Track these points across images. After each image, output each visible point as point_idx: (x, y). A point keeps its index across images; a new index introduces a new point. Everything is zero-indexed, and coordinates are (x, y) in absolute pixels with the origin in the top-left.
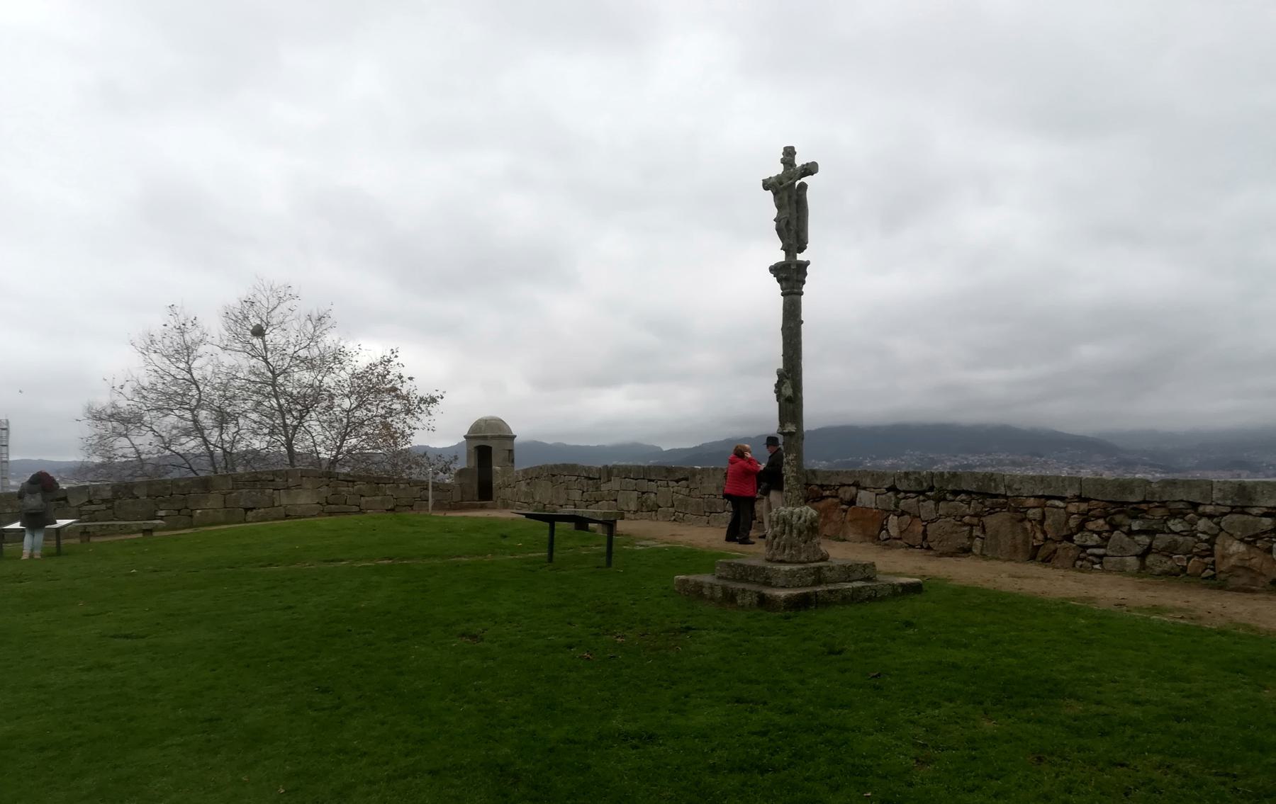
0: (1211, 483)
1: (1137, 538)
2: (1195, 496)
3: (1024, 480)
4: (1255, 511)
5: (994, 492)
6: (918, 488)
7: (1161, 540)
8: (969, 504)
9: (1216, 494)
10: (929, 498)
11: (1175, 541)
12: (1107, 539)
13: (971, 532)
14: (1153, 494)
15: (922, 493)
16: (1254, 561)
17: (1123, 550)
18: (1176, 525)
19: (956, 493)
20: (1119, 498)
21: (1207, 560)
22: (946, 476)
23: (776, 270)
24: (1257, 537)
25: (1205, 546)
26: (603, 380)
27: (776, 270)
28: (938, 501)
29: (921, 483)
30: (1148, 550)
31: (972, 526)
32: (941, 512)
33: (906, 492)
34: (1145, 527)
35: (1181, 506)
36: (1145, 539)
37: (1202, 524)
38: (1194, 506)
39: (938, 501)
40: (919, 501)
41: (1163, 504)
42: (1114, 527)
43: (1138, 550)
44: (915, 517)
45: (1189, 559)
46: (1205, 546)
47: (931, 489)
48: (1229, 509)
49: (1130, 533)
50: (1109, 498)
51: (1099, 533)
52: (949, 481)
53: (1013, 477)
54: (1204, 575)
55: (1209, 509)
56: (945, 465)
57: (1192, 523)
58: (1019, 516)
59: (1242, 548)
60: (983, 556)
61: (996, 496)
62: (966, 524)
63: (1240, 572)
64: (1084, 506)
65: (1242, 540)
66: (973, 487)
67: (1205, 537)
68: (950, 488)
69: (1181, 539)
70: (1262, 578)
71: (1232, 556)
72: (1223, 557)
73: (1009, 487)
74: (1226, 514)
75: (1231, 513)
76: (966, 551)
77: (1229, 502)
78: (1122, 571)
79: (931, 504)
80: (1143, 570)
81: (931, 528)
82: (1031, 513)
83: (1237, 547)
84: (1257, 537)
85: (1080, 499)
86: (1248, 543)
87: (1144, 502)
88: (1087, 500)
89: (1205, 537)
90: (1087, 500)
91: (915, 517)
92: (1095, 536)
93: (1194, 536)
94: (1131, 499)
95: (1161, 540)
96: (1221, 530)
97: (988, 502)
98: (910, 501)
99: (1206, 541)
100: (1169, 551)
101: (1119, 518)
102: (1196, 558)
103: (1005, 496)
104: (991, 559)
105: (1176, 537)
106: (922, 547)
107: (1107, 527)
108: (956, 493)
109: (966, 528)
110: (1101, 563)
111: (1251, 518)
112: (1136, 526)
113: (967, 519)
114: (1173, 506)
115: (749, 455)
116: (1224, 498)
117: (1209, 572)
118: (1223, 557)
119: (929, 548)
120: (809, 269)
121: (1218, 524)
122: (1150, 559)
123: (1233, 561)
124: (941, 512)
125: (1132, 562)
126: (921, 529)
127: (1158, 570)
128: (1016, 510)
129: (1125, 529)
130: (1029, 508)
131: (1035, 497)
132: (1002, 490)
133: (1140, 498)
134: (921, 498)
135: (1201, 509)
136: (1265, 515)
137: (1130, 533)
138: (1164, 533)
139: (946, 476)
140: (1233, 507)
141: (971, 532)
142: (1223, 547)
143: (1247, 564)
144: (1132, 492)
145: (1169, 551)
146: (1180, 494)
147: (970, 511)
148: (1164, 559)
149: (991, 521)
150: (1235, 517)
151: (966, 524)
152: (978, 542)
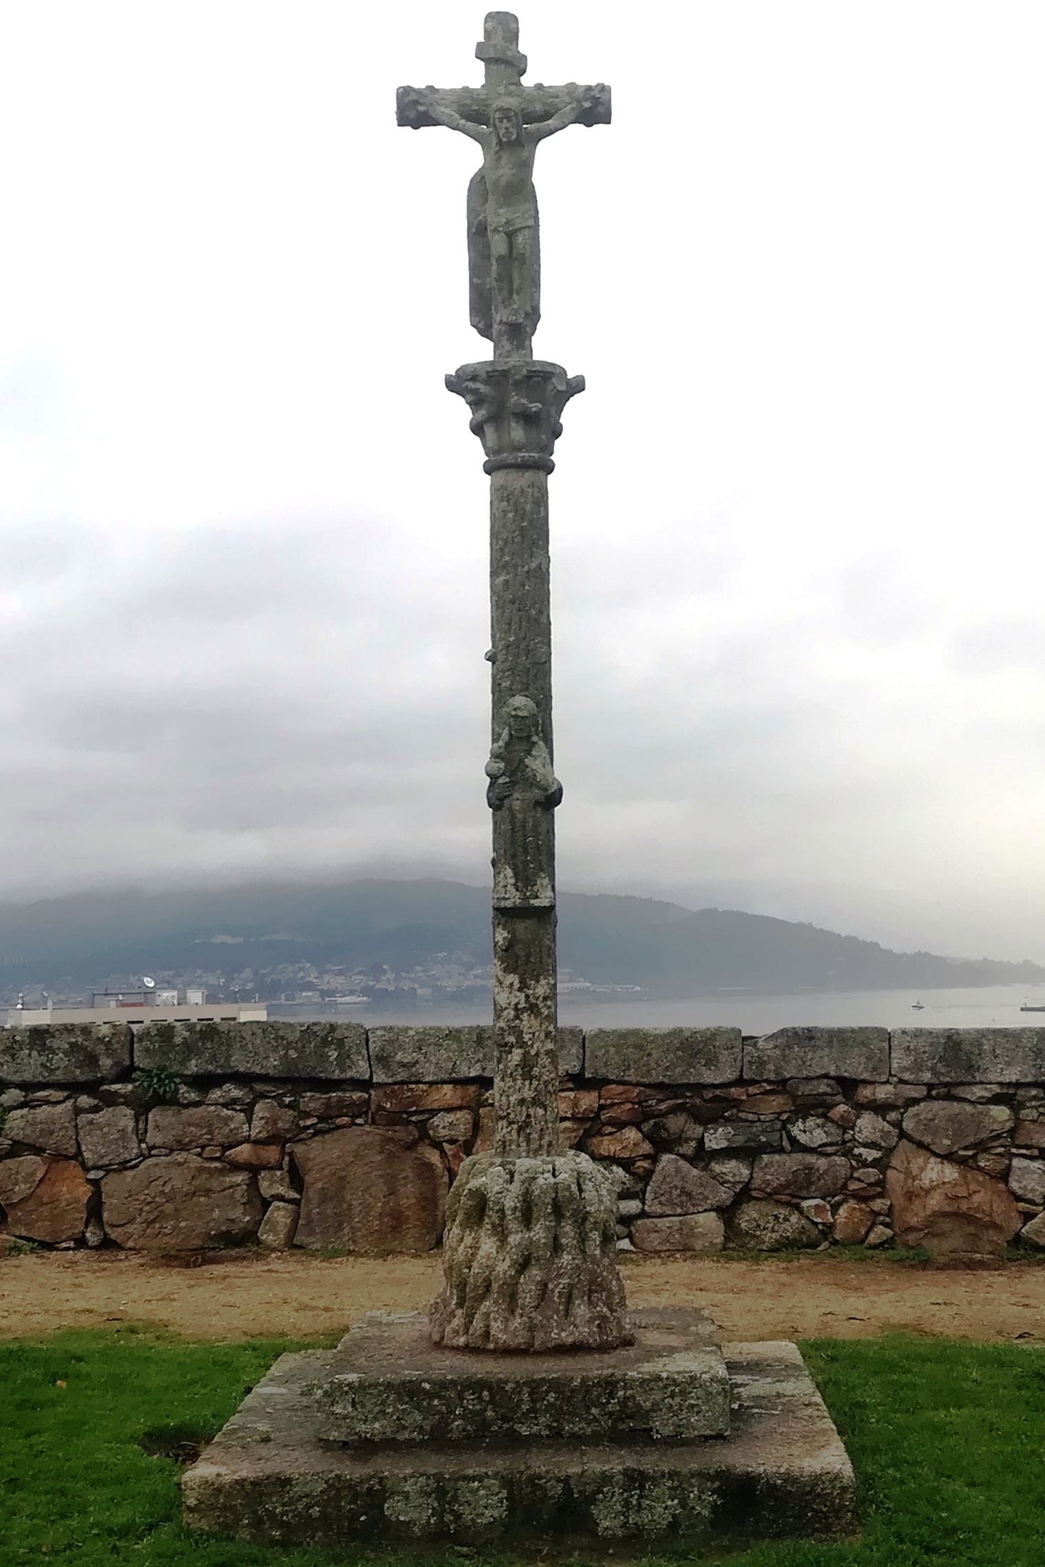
0: (889, 1037)
1: (717, 1167)
2: (854, 1067)
3: (423, 1041)
4: (979, 1092)
5: (337, 1075)
6: (80, 1075)
7: (776, 1168)
8: (249, 1111)
9: (899, 1060)
10: (111, 1100)
11: (809, 1168)
12: (649, 1173)
13: (253, 1184)
14: (762, 1063)
15: (90, 1087)
16: (977, 1198)
17: (687, 1199)
18: (811, 1132)
19: (204, 1082)
20: (678, 1075)
21: (878, 1204)
22: (181, 1034)
23: (462, 383)
24: (981, 1147)
25: (873, 1174)
26: (773, 1336)
27: (462, 383)
28: (141, 1108)
29: (91, 1060)
30: (744, 1194)
31: (254, 1169)
32: (153, 1137)
33: (25, 1086)
34: (740, 1140)
35: (823, 1088)
36: (734, 1169)
37: (868, 1126)
38: (848, 1086)
39: (141, 1108)
40: (77, 1111)
41: (781, 1085)
42: (662, 1143)
43: (724, 1195)
44: (59, 1157)
45: (835, 1208)
46: (873, 1174)
47: (125, 1074)
48: (923, 1091)
49: (702, 1156)
50: (657, 1077)
51: (626, 1164)
52: (189, 1049)
53: (394, 1036)
54: (872, 1238)
55: (883, 1093)
56: (181, 1003)
57: (846, 1125)
58: (400, 1133)
59: (950, 1173)
60: (292, 1245)
61: (337, 1084)
62: (236, 1167)
63: (946, 1225)
64: (588, 1100)
65: (948, 1157)
66: (272, 1064)
67: (871, 1155)
68: (193, 1067)
69: (821, 1163)
70: (992, 1235)
71: (928, 1192)
72: (910, 1196)
73: (383, 1060)
74: (915, 1101)
75: (929, 1097)
76: (239, 1243)
77: (927, 1076)
78: (686, 1249)
79: (124, 1117)
80: (736, 1243)
81: (111, 1185)
82: (442, 1124)
83: (936, 1173)
84: (981, 1147)
85: (578, 1081)
86: (961, 1162)
87: (740, 1082)
88: (597, 1084)
89: (871, 1155)
90: (597, 1084)
91: (59, 1157)
92: (619, 1171)
93: (848, 1153)
94: (709, 1077)
95: (776, 1168)
96: (903, 1135)
97: (312, 1101)
98: (44, 1112)
99: (875, 1163)
100: (789, 1194)
101: (676, 1123)
102: (852, 1203)
103: (366, 1085)
104: (313, 1255)
105: (811, 1159)
106: (81, 1243)
107: (647, 1148)
108: (204, 1082)
109: (240, 1178)
110: (630, 1236)
111: (968, 1108)
112: (716, 1139)
113: (243, 1152)
114: (805, 1089)
115: (664, 1375)
116: (918, 1067)
117: (880, 1233)
118: (910, 1196)
119: (107, 1245)
120: (572, 414)
121: (898, 1124)
122: (749, 1215)
123: (935, 1202)
124: (153, 1137)
125: (709, 1223)
126: (84, 1192)
127: (769, 1238)
128: (394, 1119)
129: (689, 1148)
130: (434, 1112)
131: (455, 1082)
132: (360, 1069)
133: (730, 1075)
134: (85, 1100)
135: (865, 1093)
136: (996, 1100)
137: (702, 1156)
138: (781, 1150)
139: (181, 1034)
140: (930, 1086)
141: (253, 1184)
142: (908, 1173)
143: (964, 1206)
144: (711, 1062)
145: (789, 1194)
146: (825, 1062)
147: (257, 1129)
148: (783, 1212)
149: (320, 1154)
150: (936, 1106)
151: (236, 1167)
152: (279, 1215)
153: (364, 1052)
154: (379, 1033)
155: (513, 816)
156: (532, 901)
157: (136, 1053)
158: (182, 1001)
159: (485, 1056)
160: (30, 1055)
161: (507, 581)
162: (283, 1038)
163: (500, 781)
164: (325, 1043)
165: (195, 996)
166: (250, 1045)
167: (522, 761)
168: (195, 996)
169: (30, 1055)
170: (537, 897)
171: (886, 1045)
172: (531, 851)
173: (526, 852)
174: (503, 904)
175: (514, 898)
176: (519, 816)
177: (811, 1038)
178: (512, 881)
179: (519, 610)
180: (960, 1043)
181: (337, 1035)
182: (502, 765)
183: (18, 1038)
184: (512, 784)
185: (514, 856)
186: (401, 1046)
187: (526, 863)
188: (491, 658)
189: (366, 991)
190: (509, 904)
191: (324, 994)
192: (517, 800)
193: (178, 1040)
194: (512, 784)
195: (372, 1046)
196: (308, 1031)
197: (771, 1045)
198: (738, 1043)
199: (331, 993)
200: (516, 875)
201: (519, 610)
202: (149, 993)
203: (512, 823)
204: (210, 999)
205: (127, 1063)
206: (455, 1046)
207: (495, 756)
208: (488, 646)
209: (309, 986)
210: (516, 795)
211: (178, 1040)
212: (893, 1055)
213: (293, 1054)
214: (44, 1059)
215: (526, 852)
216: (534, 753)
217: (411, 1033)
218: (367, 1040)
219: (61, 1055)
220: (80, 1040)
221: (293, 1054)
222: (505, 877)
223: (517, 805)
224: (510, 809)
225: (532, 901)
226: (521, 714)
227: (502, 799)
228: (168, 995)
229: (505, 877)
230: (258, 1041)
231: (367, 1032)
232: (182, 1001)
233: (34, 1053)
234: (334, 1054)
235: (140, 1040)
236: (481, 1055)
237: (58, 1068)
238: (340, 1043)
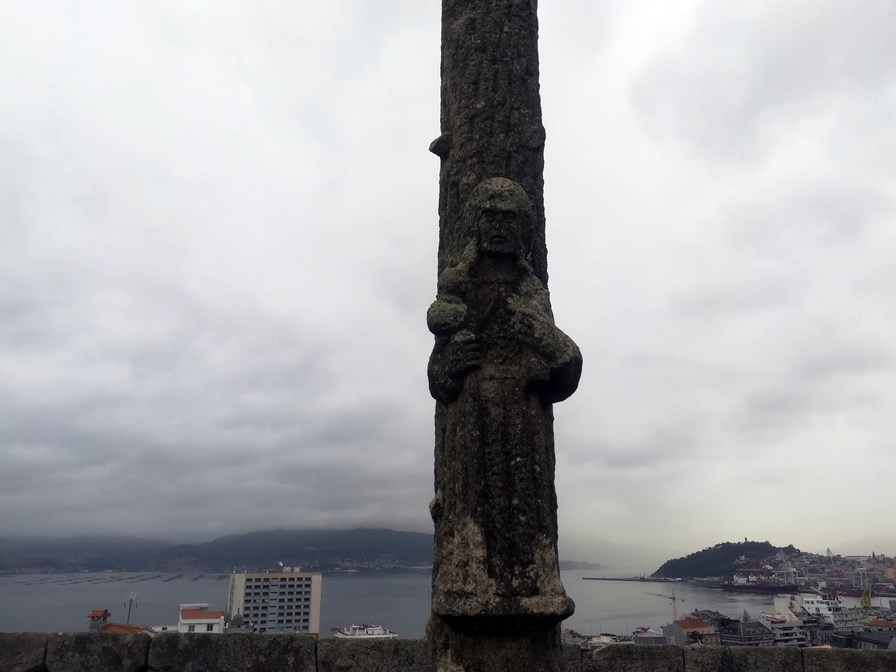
153: (313, 658)
154: (325, 644)
155: (482, 412)
156: (526, 602)
157: (150, 656)
158: (292, 571)
159: (399, 663)
160: (73, 656)
161: (473, 20)
162: (256, 646)
163: (459, 338)
164: (286, 651)
165: (297, 569)
166: (232, 652)
167: (501, 302)
168: (297, 569)
169: (73, 656)
170: (534, 591)
171: (681, 658)
172: (519, 486)
173: (509, 489)
174: (461, 607)
175: (483, 595)
176: (494, 411)
177: (630, 653)
178: (480, 553)
179: (494, 61)
180: (732, 658)
181: (295, 645)
182: (462, 308)
183: (66, 643)
184: (481, 347)
185: (485, 496)
186: (340, 654)
187: (510, 512)
188: (438, 148)
189: (357, 568)
190: (472, 607)
191: (343, 569)
192: (491, 380)
193: (181, 647)
194: (481, 347)
195: (319, 653)
196: (275, 641)
197: (602, 657)
198: (579, 656)
199: (346, 569)
200: (489, 536)
201: (494, 61)
202: (281, 568)
203: (483, 430)
204: (302, 571)
205: (142, 663)
206: (378, 654)
207: (446, 289)
208: (436, 133)
209: (338, 566)
210: (489, 370)
211: (181, 647)
212: (687, 666)
213: (262, 659)
214: (83, 658)
215: (509, 489)
216: (524, 288)
217: (348, 644)
218: (316, 649)
219: (96, 656)
220: (111, 645)
221: (262, 659)
222: (465, 544)
223: (489, 389)
224: (477, 397)
225: (526, 602)
226: (501, 205)
227: (459, 376)
228: (288, 569)
229: (465, 544)
230: (238, 649)
231: (316, 642)
232: (292, 571)
233: (77, 655)
234: (291, 660)
235: (154, 647)
236: (396, 662)
237: (92, 667)
238: (297, 651)
